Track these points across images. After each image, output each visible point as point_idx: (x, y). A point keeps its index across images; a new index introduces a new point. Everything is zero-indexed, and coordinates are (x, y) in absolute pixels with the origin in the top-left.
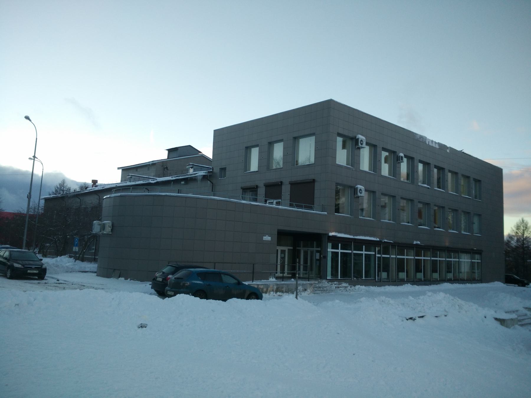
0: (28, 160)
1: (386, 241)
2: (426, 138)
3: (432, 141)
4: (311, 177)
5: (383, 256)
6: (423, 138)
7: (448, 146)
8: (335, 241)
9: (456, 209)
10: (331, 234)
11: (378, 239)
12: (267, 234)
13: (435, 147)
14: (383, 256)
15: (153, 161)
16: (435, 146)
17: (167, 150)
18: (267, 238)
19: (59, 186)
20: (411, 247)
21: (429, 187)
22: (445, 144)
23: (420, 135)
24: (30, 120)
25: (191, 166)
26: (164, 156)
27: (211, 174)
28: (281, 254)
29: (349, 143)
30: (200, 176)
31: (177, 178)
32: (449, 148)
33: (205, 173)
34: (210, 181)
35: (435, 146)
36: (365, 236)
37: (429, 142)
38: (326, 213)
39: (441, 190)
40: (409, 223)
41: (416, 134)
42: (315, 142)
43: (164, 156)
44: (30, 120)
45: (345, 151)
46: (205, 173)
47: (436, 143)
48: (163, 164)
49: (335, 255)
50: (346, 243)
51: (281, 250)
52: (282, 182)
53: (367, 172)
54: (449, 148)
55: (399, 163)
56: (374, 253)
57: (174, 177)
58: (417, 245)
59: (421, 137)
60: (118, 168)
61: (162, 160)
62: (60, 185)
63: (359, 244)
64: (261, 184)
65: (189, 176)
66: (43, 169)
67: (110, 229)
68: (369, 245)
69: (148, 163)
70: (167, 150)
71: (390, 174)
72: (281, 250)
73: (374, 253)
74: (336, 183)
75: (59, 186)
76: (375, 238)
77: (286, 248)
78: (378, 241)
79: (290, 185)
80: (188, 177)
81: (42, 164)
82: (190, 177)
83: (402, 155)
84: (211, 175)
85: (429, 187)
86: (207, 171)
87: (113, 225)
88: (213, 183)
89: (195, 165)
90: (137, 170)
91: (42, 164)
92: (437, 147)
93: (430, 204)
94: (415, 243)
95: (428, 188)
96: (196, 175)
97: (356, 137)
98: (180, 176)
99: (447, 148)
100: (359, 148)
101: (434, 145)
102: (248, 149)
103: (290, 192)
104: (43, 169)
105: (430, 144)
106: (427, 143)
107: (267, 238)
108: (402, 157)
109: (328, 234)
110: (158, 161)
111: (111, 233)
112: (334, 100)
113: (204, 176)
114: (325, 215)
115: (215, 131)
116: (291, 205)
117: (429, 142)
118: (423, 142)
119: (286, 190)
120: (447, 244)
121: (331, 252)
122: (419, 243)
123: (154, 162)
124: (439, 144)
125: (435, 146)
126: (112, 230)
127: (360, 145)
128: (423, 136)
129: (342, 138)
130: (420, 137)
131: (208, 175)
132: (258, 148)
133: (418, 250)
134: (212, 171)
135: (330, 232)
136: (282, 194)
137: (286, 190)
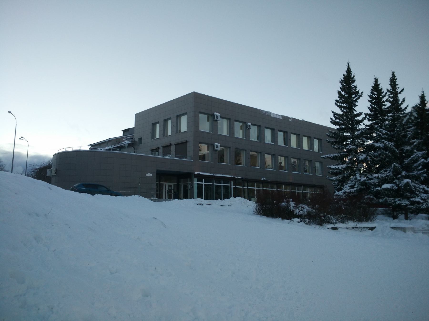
0: (19, 140)
1: (238, 177)
2: (271, 112)
3: (276, 115)
4: (186, 139)
5: (237, 187)
6: (268, 113)
7: (290, 117)
8: (200, 178)
9: (299, 158)
10: (196, 173)
11: (233, 177)
12: (149, 172)
13: (279, 119)
14: (237, 187)
15: (109, 139)
16: (279, 117)
17: (122, 131)
18: (149, 175)
19: (50, 161)
20: (259, 182)
21: (274, 144)
22: (288, 116)
23: (266, 111)
24: (12, 114)
25: (126, 139)
26: (121, 134)
27: (133, 142)
28: (168, 187)
29: (211, 118)
30: (127, 144)
31: (114, 146)
32: (291, 119)
33: (130, 142)
34: (133, 147)
35: (279, 117)
36: (222, 175)
37: (273, 115)
38: (193, 160)
39: (286, 146)
40: (259, 167)
41: (262, 110)
42: (187, 118)
43: (121, 134)
44: (12, 114)
45: (209, 123)
46: (130, 142)
47: (279, 116)
48: (117, 140)
49: (200, 187)
50: (208, 179)
51: (168, 185)
52: (171, 144)
53: (226, 136)
54: (291, 119)
55: (248, 129)
56: (230, 185)
57: (113, 146)
58: (264, 180)
59: (267, 112)
60: (88, 145)
61: (116, 137)
62: (51, 160)
63: (218, 179)
64: (160, 146)
65: (121, 145)
66: (28, 145)
67: (55, 172)
68: (227, 180)
69: (106, 140)
70: (122, 131)
71: (243, 137)
72: (168, 185)
73: (230, 185)
74: (235, 149)
75: (50, 161)
76: (230, 176)
77: (172, 184)
78: (232, 177)
79: (175, 145)
80: (120, 145)
81: (27, 141)
82: (122, 145)
83: (249, 124)
84: (134, 143)
85: (274, 144)
86: (131, 141)
87: (56, 170)
88: (135, 148)
89: (128, 138)
90: (100, 146)
91: (27, 141)
92: (281, 118)
93: (322, 162)
94: (262, 179)
95: (273, 145)
96: (125, 144)
97: (214, 114)
98: (116, 145)
99: (290, 118)
100: (217, 121)
101: (278, 117)
102: (154, 125)
103: (175, 149)
104: (28, 145)
105: (275, 116)
106: (272, 116)
107: (149, 175)
108: (249, 126)
109: (194, 173)
110: (113, 139)
111: (55, 175)
112: (196, 92)
113: (129, 144)
114: (192, 161)
115: (135, 114)
116: (176, 157)
117: (273, 115)
118: (268, 115)
119: (173, 148)
120: (291, 181)
121: (197, 184)
122: (265, 179)
123: (110, 139)
124: (282, 116)
125: (279, 118)
126: (55, 173)
127: (216, 119)
128: (268, 112)
129: (207, 115)
130: (265, 112)
131: (132, 143)
132: (159, 124)
133: (266, 183)
134: (134, 140)
135: (196, 172)
136: (172, 151)
137: (173, 148)
